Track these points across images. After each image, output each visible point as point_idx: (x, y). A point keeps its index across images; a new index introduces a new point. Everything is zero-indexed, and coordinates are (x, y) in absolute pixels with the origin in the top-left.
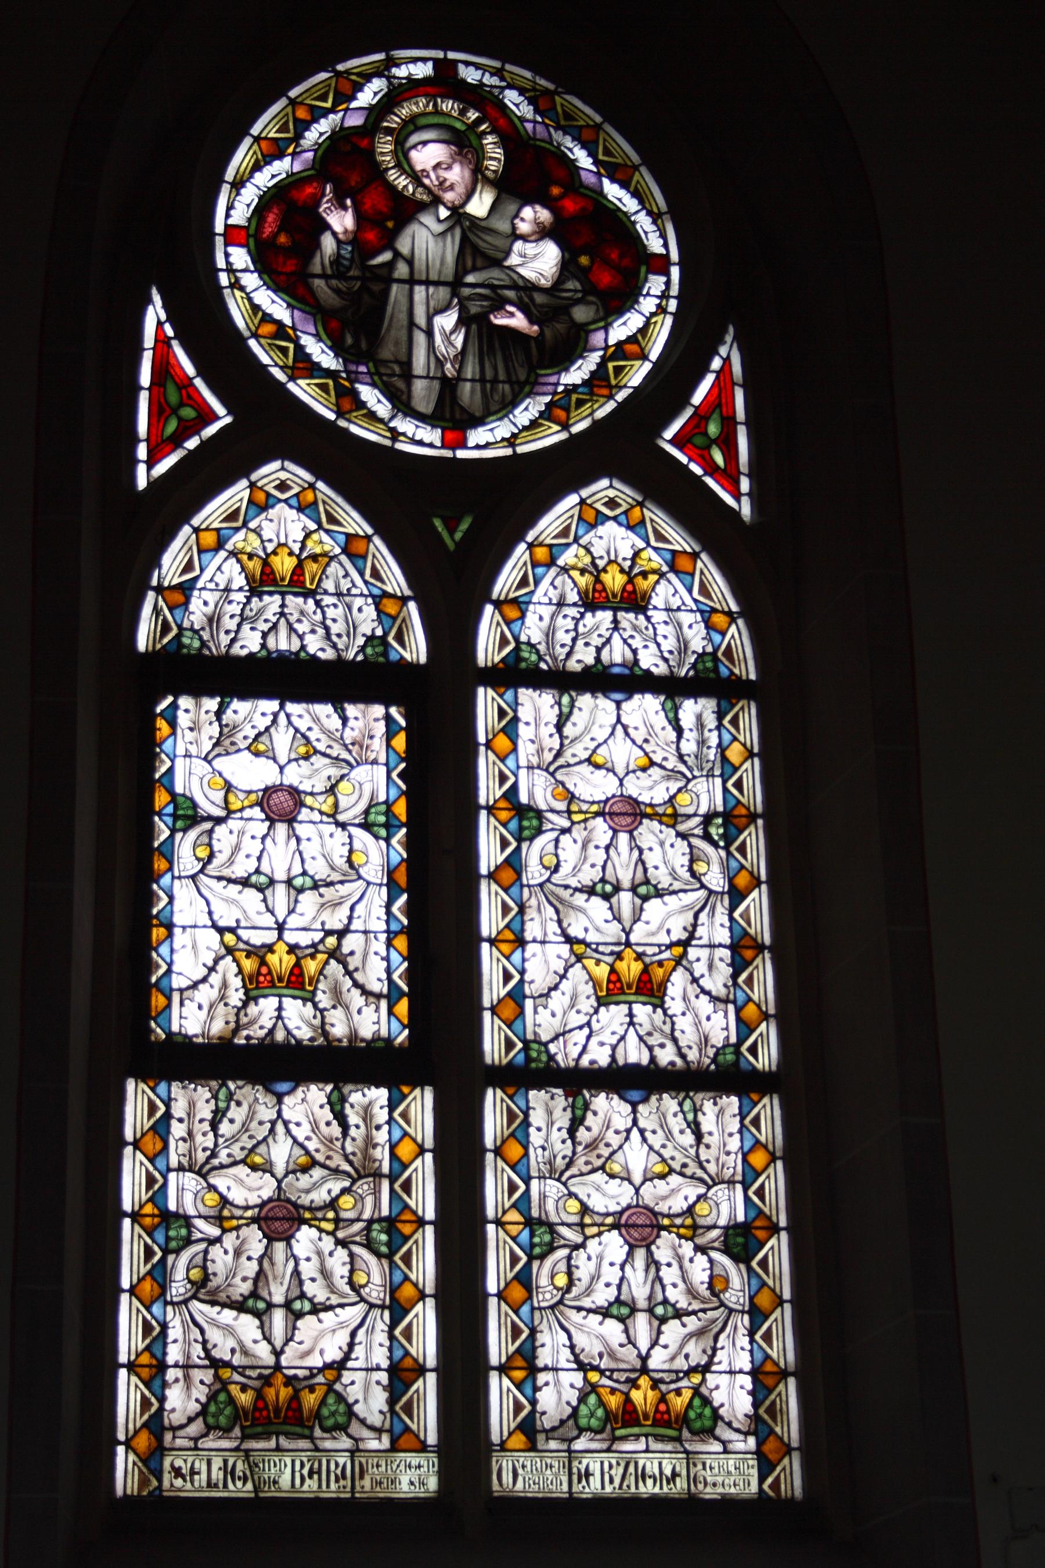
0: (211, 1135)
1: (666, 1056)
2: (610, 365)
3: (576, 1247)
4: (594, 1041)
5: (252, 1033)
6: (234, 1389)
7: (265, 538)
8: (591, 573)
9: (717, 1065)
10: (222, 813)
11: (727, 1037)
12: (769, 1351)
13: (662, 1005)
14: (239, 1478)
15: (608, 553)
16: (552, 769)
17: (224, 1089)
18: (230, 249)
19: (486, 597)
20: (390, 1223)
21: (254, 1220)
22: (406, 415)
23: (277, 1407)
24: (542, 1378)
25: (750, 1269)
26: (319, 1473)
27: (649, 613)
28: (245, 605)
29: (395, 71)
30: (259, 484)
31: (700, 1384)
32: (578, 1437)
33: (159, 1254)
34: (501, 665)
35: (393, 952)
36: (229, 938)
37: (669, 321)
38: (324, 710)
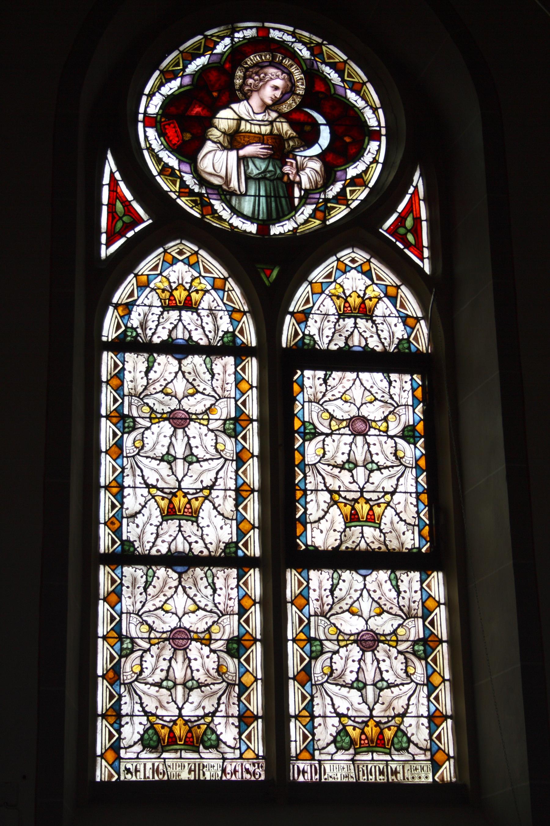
0: (330, 597)
1: (198, 548)
2: (348, 189)
3: (145, 651)
4: (159, 540)
5: (348, 545)
6: (350, 729)
7: (171, 281)
8: (168, 291)
9: (225, 554)
10: (329, 431)
11: (231, 538)
12: (437, 706)
13: (197, 522)
14: (161, 774)
15: (178, 280)
16: (321, 403)
17: (151, 570)
18: (147, 129)
19: (109, 302)
20: (424, 641)
21: (355, 641)
22: (238, 216)
23: (383, 738)
24: (124, 720)
25: (427, 663)
26: (195, 771)
27: (199, 311)
28: (336, 323)
29: (236, 35)
30: (341, 260)
31: (210, 723)
32: (336, 753)
33: (308, 659)
34: (294, 347)
35: (420, 503)
36: (336, 497)
37: (380, 166)
38: (379, 376)
